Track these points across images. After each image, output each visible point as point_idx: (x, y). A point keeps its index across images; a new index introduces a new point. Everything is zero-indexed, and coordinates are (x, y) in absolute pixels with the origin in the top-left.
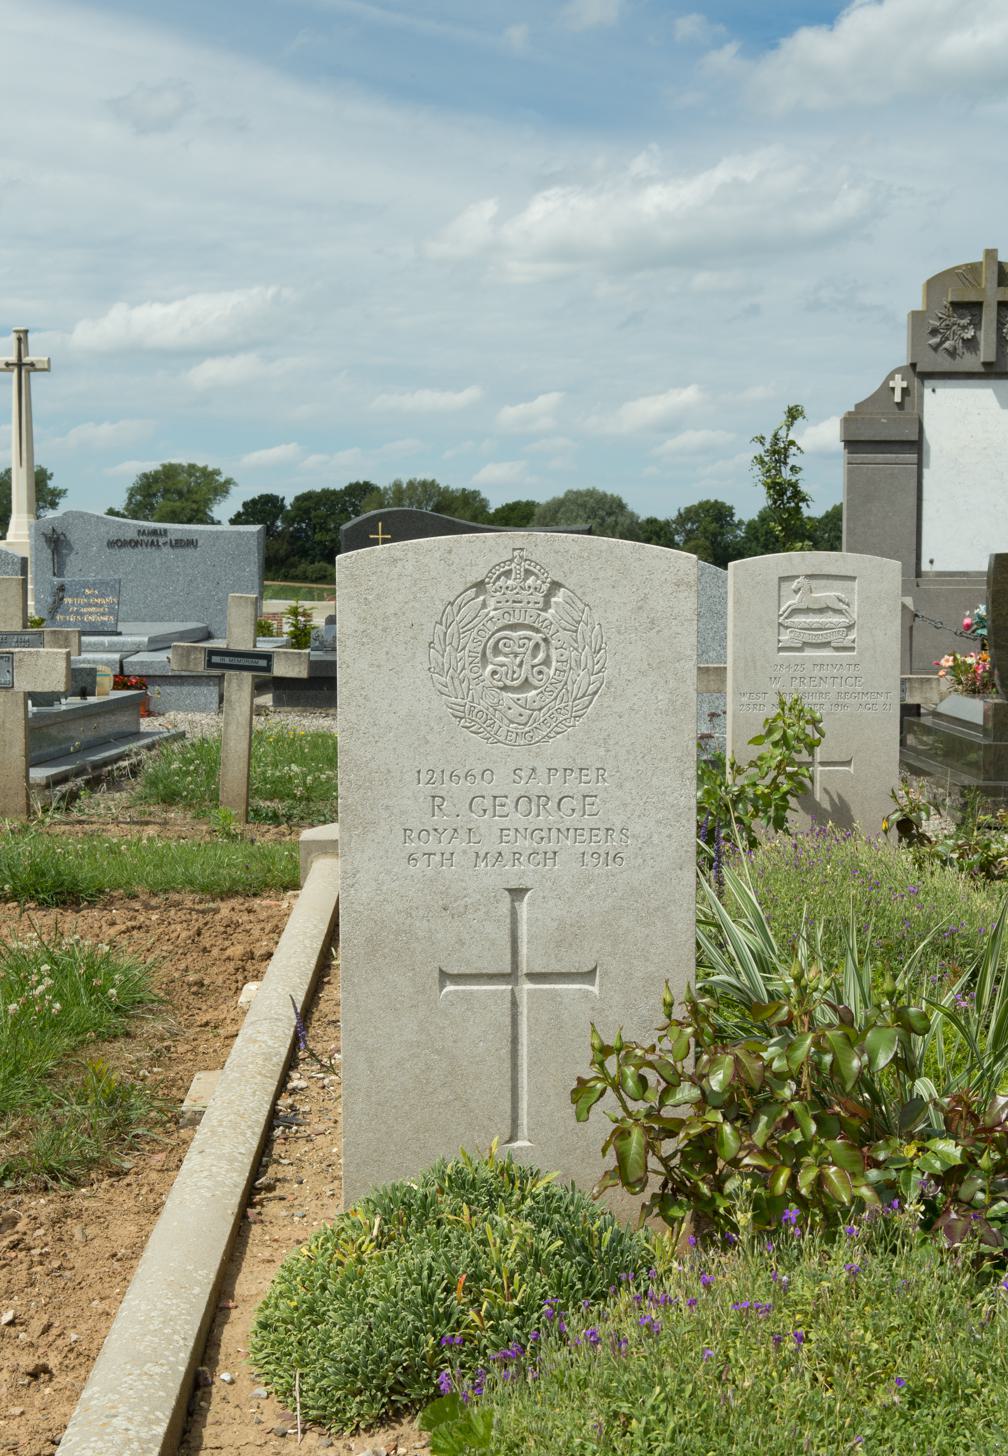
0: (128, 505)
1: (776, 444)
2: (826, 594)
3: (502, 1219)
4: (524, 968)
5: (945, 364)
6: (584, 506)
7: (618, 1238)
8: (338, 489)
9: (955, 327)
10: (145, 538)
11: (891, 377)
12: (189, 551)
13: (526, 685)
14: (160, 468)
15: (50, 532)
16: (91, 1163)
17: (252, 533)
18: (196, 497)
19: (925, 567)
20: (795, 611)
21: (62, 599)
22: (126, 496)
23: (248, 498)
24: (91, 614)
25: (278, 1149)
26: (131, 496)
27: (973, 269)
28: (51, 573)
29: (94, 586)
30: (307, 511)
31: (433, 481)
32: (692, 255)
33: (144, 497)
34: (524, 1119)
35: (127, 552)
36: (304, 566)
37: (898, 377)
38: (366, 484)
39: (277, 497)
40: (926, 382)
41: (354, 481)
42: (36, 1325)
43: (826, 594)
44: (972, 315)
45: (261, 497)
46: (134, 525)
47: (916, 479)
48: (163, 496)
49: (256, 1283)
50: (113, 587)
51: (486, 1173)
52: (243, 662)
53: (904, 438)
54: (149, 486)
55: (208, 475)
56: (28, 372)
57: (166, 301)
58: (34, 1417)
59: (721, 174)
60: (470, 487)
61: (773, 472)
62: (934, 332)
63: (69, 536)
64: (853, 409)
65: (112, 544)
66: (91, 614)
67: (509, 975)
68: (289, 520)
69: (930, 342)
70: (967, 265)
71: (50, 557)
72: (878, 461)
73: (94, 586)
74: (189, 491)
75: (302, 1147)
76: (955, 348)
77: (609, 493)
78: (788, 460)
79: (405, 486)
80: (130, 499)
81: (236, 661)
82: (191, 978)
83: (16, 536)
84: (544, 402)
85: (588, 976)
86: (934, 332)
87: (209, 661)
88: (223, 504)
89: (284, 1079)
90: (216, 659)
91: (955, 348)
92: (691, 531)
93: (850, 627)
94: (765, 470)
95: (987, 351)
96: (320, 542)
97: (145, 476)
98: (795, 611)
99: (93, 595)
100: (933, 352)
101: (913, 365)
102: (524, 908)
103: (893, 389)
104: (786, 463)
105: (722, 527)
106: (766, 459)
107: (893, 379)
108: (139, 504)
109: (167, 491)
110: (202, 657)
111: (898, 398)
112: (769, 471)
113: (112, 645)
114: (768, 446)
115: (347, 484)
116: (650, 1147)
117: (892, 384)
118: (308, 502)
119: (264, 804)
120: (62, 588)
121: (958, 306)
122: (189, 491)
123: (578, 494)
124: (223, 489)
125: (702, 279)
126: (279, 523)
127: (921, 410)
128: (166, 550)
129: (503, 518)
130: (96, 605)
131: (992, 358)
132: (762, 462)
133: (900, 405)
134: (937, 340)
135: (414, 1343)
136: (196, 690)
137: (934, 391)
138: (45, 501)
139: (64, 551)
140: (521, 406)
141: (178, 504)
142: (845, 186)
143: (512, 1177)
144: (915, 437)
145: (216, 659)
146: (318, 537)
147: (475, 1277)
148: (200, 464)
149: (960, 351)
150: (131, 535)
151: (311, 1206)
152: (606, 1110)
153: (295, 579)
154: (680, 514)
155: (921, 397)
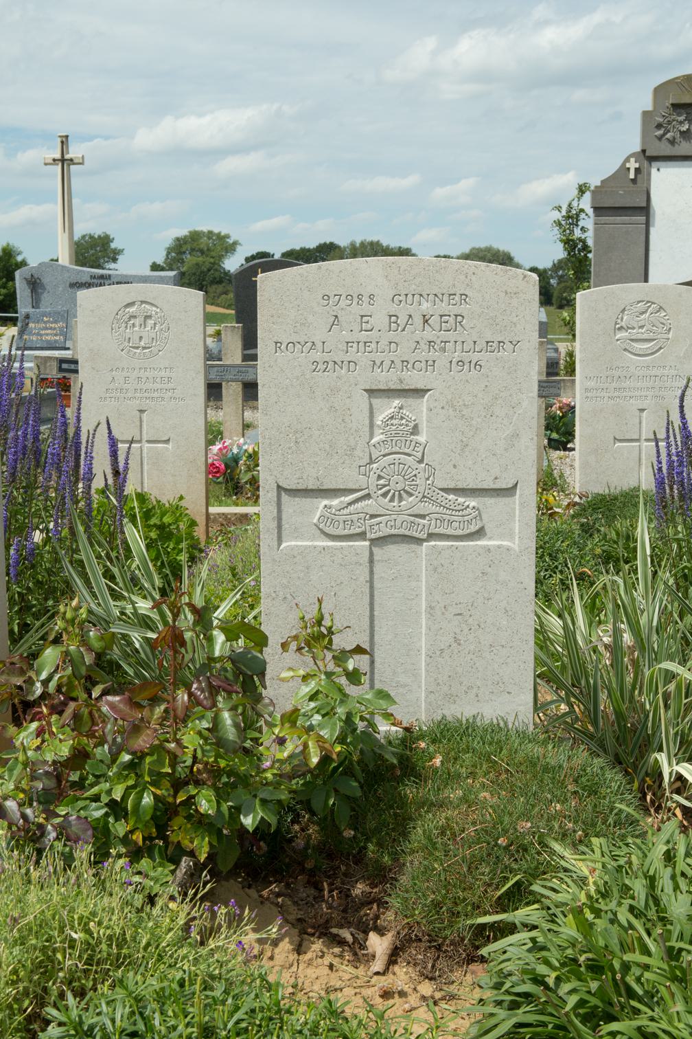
0: (166, 259)
1: (570, 211)
4: (145, 438)
5: (666, 149)
8: (312, 247)
9: (674, 123)
10: (95, 281)
11: (627, 160)
14: (188, 234)
15: (30, 277)
17: (170, 277)
18: (213, 254)
21: (27, 324)
22: (164, 253)
24: (47, 335)
26: (168, 253)
28: (30, 306)
32: (571, 78)
33: (177, 254)
37: (632, 160)
38: (331, 244)
40: (654, 164)
44: (687, 114)
46: (88, 272)
47: (644, 235)
48: (190, 253)
50: (63, 316)
53: (636, 205)
55: (221, 238)
56: (69, 165)
57: (201, 115)
59: (597, 17)
61: (568, 231)
62: (659, 126)
63: (43, 280)
64: (599, 184)
66: (47, 335)
69: (656, 134)
70: (684, 76)
71: (30, 295)
72: (608, 222)
74: (208, 250)
76: (674, 138)
77: (501, 248)
78: (579, 223)
79: (358, 245)
80: (167, 255)
84: (466, 184)
86: (659, 126)
87: (60, 367)
88: (231, 259)
90: (65, 366)
91: (674, 138)
92: (562, 276)
94: (561, 231)
97: (178, 239)
99: (48, 321)
100: (657, 141)
101: (644, 151)
103: (629, 169)
104: (577, 225)
106: (563, 223)
107: (629, 161)
108: (174, 259)
109: (193, 250)
110: (55, 364)
111: (632, 176)
112: (565, 231)
114: (564, 213)
115: (317, 244)
117: (628, 165)
122: (208, 250)
124: (231, 248)
125: (579, 95)
127: (649, 184)
130: (51, 328)
132: (559, 224)
133: (634, 181)
134: (661, 132)
137: (658, 170)
138: (109, 258)
139: (40, 291)
140: (448, 187)
141: (201, 259)
142: (688, 25)
144: (644, 204)
145: (65, 366)
148: (216, 231)
149: (678, 140)
150: (86, 279)
154: (554, 265)
155: (649, 174)
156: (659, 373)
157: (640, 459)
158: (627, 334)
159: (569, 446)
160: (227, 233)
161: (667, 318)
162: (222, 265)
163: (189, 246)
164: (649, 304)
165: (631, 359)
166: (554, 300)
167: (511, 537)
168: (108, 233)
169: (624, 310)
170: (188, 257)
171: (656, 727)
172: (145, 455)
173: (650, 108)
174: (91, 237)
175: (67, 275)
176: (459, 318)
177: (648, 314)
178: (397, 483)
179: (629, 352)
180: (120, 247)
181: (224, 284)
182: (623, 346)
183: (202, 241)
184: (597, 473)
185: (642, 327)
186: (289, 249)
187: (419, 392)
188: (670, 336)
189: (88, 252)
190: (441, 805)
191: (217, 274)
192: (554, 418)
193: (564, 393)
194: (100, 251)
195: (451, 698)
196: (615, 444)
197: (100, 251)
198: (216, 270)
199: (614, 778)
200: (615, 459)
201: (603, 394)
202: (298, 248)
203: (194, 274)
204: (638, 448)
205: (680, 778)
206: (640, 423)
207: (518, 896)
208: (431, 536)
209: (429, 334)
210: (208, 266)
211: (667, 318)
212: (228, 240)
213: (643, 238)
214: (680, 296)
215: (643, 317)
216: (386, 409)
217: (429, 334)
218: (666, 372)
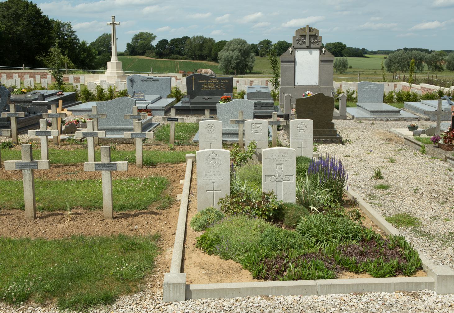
2: (258, 126)
3: (212, 213)
4: (214, 190)
6: (237, 42)
7: (222, 215)
12: (157, 82)
13: (214, 164)
16: (168, 206)
18: (147, 40)
19: (296, 84)
20: (254, 128)
25: (189, 205)
26: (133, 40)
27: (304, 29)
29: (140, 91)
30: (173, 43)
34: (214, 204)
35: (145, 82)
36: (173, 56)
38: (187, 37)
41: (265, 39)
42: (168, 223)
43: (258, 126)
45: (163, 40)
49: (190, 219)
51: (211, 209)
52: (173, 120)
54: (137, 37)
55: (150, 35)
56: (115, 25)
58: (171, 231)
62: (297, 40)
65: (142, 81)
68: (169, 45)
73: (140, 91)
75: (192, 205)
77: (243, 39)
81: (172, 120)
82: (173, 179)
83: (113, 61)
85: (220, 190)
86: (297, 40)
89: (189, 197)
90: (169, 119)
92: (262, 47)
93: (261, 130)
95: (307, 44)
96: (176, 50)
97: (136, 35)
98: (254, 128)
102: (214, 184)
105: (269, 46)
109: (141, 39)
111: (291, 53)
113: (144, 103)
116: (224, 208)
118: (174, 41)
119: (176, 141)
120: (134, 92)
121: (302, 36)
122: (146, 39)
123: (236, 39)
124: (154, 38)
128: (153, 82)
131: (308, 45)
133: (291, 54)
134: (298, 42)
135: (205, 224)
136: (160, 112)
140: (220, 17)
143: (213, 209)
144: (294, 60)
145: (169, 119)
146: (176, 49)
147: (210, 218)
148: (149, 32)
151: (194, 211)
152: (221, 205)
153: (171, 59)
166: (259, 54)
167: (293, 180)
170: (139, 41)
171: (310, 202)
173: (295, 35)
174: (107, 34)
175: (141, 78)
178: (279, 175)
186: (173, 38)
187: (282, 164)
190: (288, 213)
195: (286, 200)
199: (306, 209)
205: (313, 209)
207: (298, 222)
208: (283, 181)
209: (283, 157)
210: (146, 44)
213: (294, 68)
216: (278, 166)
217: (283, 157)
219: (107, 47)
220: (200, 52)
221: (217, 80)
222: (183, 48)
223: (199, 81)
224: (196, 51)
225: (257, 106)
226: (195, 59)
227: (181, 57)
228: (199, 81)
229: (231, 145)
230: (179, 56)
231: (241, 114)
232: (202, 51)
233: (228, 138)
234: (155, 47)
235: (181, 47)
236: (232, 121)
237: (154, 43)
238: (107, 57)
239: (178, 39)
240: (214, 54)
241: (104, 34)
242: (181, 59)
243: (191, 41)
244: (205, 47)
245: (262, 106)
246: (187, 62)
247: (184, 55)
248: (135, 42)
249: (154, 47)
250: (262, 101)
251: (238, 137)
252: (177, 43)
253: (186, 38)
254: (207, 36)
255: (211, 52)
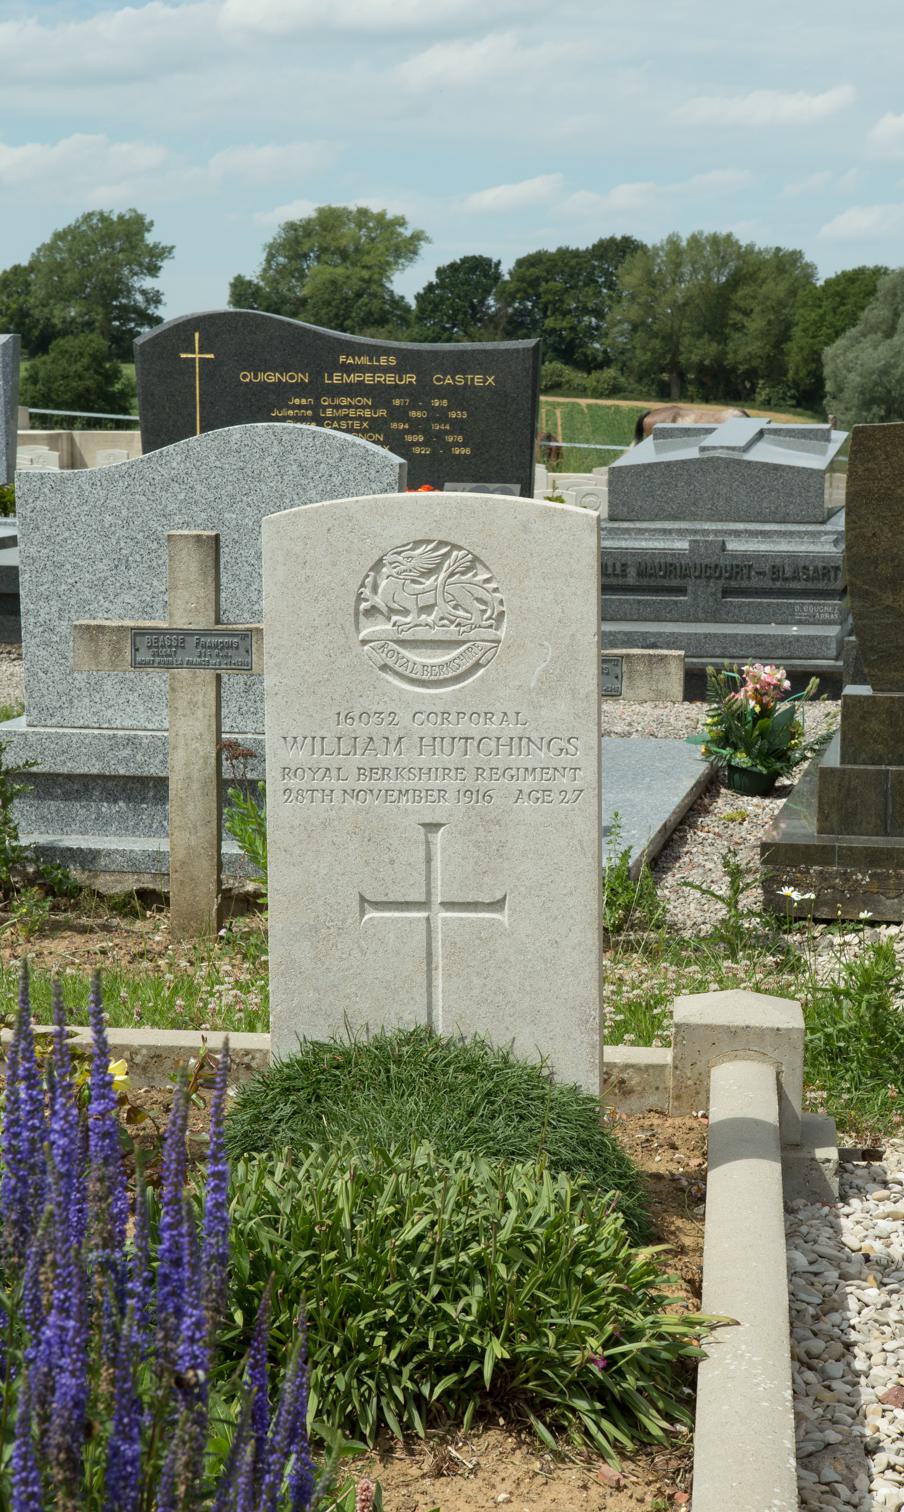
0: (265, 270)
8: (582, 248)
18: (367, 260)
23: (445, 262)
26: (270, 257)
30: (534, 283)
31: (729, 236)
33: (290, 259)
39: (488, 261)
45: (465, 260)
48: (318, 258)
54: (297, 242)
55: (386, 226)
60: (789, 245)
67: (424, 903)
68: (507, 297)
74: (357, 250)
88: (408, 271)
97: (291, 227)
109: (324, 250)
118: (535, 267)
122: (357, 250)
124: (407, 248)
126: (491, 301)
129: (837, 294)
138: (140, 265)
141: (340, 270)
148: (375, 209)
156: (475, 729)
157: (429, 955)
158: (389, 627)
159: (777, 784)
160: (399, 213)
161: (493, 585)
162: (388, 285)
163: (315, 242)
164: (444, 551)
165: (401, 691)
168: (140, 212)
169: (378, 565)
170: (312, 266)
172: (439, 937)
174: (103, 218)
176: (489, 715)
177: (443, 575)
179: (397, 673)
180: (165, 243)
181: (389, 327)
182: (381, 658)
183: (344, 230)
184: (316, 990)
185: (427, 609)
188: (502, 634)
189: (96, 252)
191: (375, 305)
192: (741, 717)
193: (631, 687)
194: (122, 250)
196: (363, 912)
197: (122, 250)
198: (374, 295)
200: (364, 953)
201: (326, 784)
202: (553, 249)
203: (328, 303)
204: (423, 926)
206: (429, 860)
210: (356, 285)
211: (493, 585)
212: (401, 230)
214: (525, 529)
215: (429, 582)
218: (493, 728)
219: (107, 306)
220: (713, 348)
221: (398, 370)
222: (598, 313)
223: (247, 377)
224: (686, 341)
225: (682, 591)
226: (675, 391)
227: (579, 377)
228: (247, 377)
229: (151, 899)
230: (568, 373)
231: (190, 564)
232: (724, 339)
233: (134, 831)
234: (413, 303)
235: (586, 311)
236: (93, 633)
237: (409, 282)
238: (85, 361)
239: (563, 253)
240: (805, 361)
241: (88, 217)
242: (582, 392)
243: (649, 272)
244: (747, 313)
245: (726, 593)
246: (617, 408)
247: (600, 366)
248: (282, 271)
249: (407, 309)
250: (733, 545)
251: (162, 831)
252: (558, 284)
253: (619, 249)
254: (759, 233)
255: (786, 346)
